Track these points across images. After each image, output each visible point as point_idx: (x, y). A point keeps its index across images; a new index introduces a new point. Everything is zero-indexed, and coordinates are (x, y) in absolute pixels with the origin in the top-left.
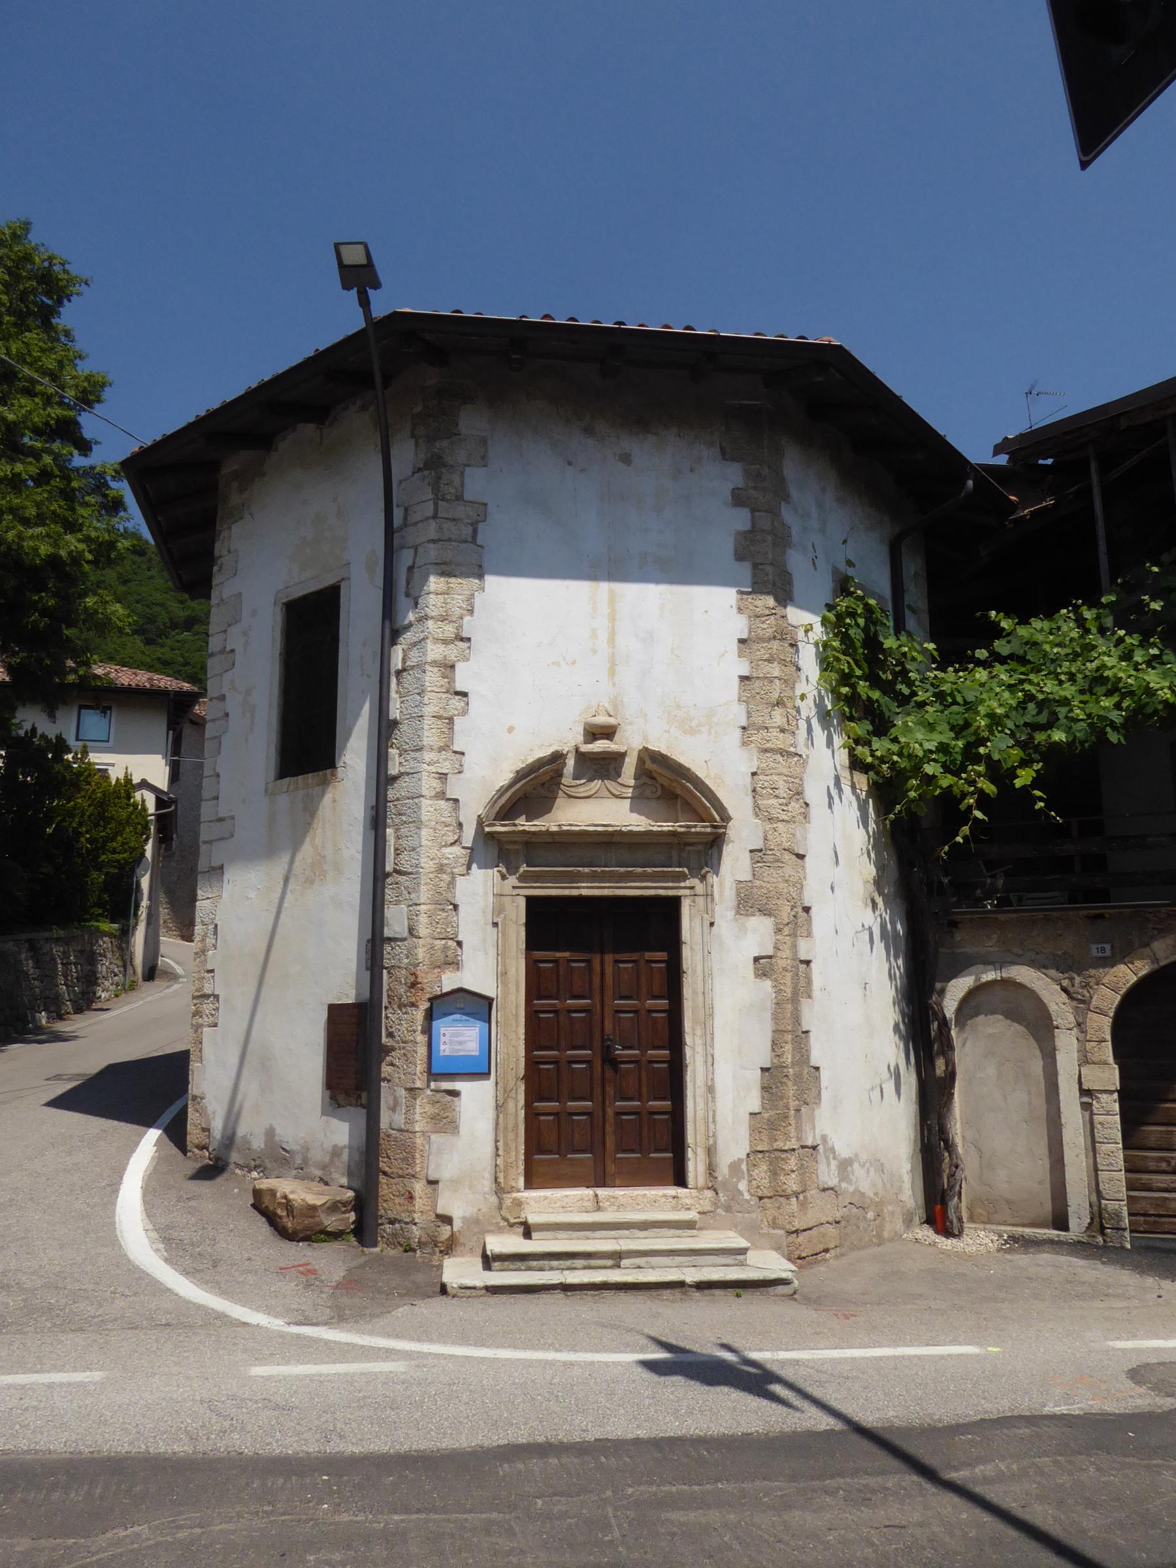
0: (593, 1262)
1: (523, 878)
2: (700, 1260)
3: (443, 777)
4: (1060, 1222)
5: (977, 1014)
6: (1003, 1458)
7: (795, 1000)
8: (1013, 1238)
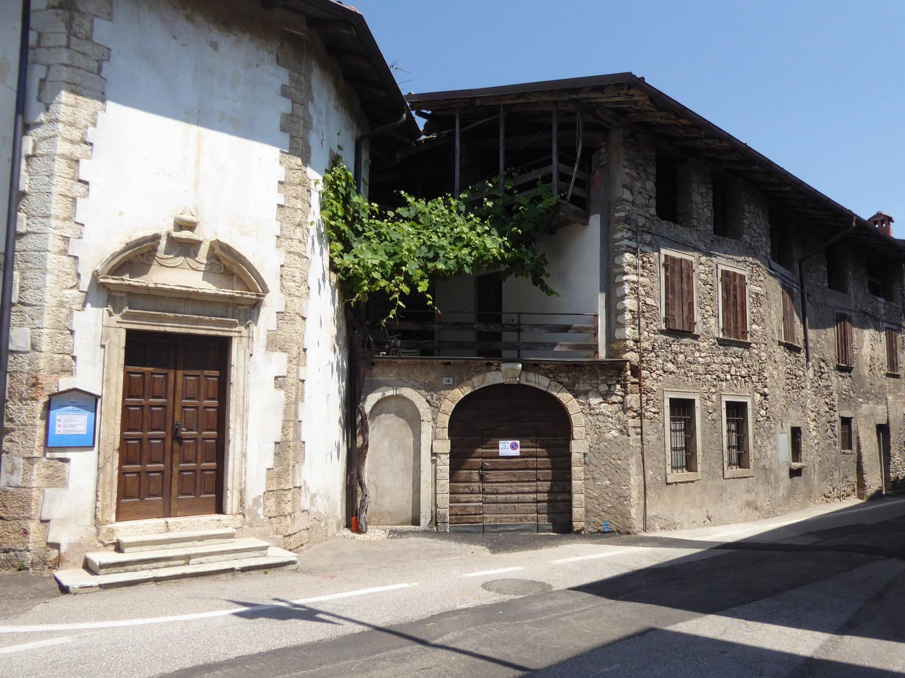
0: (171, 563)
1: (123, 317)
2: (240, 555)
3: (66, 239)
4: (416, 521)
5: (381, 414)
6: (454, 631)
7: (296, 403)
8: (391, 531)
